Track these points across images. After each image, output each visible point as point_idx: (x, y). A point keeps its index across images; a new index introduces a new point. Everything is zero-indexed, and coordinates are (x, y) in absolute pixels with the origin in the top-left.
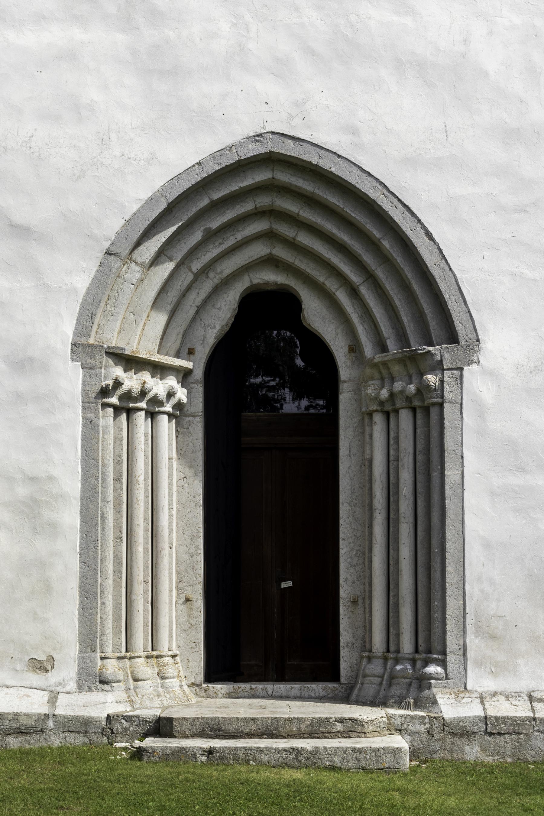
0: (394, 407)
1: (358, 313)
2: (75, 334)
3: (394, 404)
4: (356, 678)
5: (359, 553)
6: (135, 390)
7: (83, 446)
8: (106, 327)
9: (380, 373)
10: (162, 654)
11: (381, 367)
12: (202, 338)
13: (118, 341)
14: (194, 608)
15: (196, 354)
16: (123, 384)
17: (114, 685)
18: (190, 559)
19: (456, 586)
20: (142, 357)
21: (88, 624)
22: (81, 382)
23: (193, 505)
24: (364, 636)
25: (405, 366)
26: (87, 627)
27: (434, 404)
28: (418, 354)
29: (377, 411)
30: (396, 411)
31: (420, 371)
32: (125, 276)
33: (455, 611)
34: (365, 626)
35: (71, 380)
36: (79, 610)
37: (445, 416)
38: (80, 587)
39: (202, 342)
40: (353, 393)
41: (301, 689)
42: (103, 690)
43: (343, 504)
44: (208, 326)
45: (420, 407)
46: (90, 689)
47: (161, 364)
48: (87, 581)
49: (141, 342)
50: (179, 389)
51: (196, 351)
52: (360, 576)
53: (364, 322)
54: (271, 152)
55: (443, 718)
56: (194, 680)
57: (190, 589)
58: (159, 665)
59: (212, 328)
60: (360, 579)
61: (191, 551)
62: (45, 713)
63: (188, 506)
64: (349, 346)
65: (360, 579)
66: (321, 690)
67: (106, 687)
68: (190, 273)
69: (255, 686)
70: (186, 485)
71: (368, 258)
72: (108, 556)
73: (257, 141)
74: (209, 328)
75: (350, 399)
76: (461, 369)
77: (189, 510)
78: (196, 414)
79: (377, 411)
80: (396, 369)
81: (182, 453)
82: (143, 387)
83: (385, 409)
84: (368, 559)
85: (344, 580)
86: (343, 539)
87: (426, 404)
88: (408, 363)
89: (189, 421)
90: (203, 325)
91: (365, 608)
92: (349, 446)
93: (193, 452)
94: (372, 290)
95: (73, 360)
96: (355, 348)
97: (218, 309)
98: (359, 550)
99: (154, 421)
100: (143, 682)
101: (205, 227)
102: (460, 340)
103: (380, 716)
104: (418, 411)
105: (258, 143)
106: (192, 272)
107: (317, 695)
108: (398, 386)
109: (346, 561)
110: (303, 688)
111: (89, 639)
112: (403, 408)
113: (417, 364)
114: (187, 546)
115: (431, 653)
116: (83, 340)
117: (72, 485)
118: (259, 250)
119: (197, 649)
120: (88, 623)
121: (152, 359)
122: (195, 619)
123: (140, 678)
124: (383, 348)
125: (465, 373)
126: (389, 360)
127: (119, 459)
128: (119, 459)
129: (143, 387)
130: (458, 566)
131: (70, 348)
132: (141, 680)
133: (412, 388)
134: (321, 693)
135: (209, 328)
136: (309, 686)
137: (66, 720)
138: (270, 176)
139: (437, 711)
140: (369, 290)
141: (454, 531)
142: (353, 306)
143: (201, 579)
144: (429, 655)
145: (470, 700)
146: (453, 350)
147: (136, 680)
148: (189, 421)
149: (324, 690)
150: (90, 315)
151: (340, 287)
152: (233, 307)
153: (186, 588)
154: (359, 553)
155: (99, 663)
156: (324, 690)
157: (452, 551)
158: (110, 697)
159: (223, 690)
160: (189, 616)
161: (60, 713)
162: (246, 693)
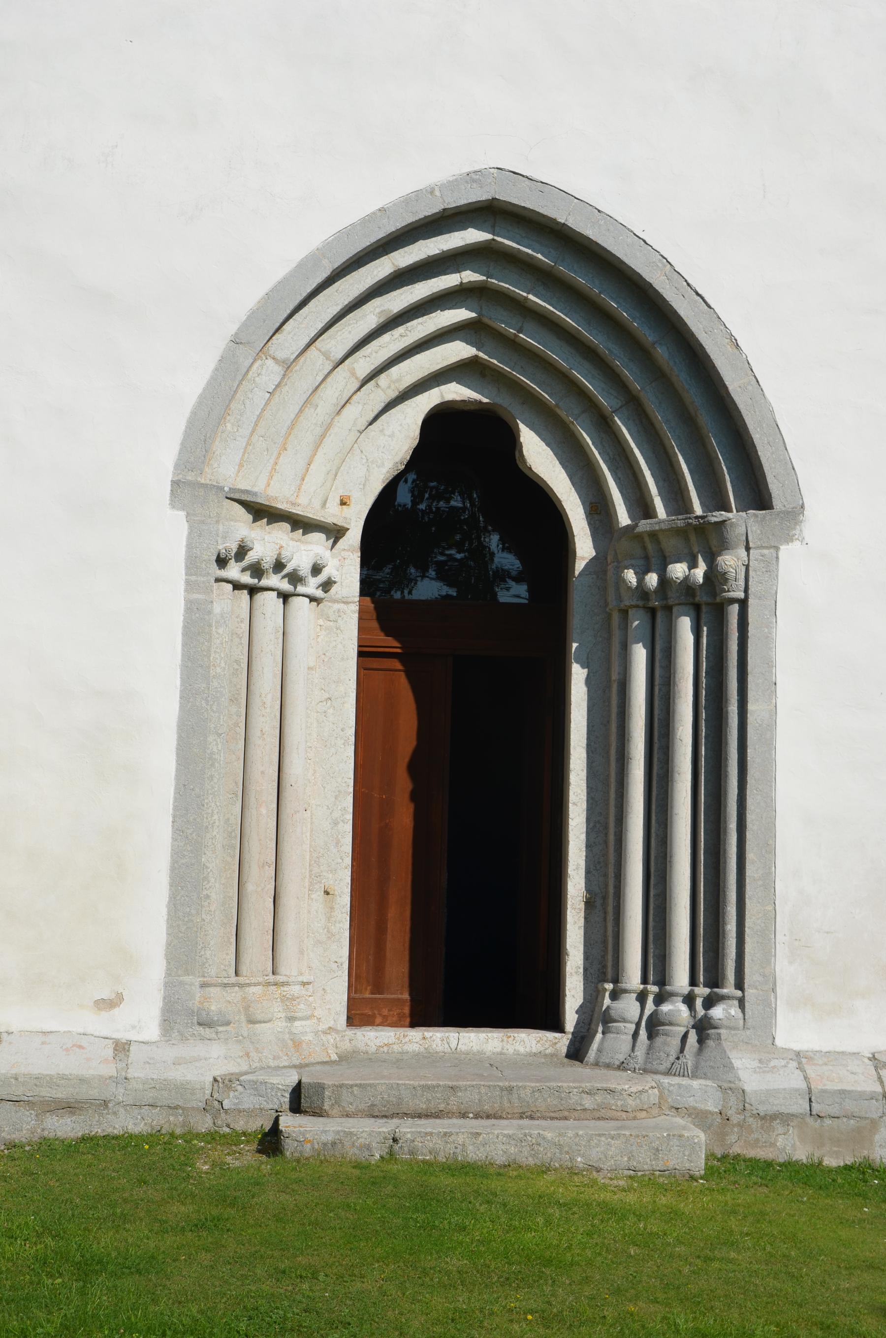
0: (665, 602)
1: (608, 454)
2: (177, 466)
3: (665, 598)
4: (590, 1024)
5: (598, 826)
6: (268, 559)
7: (185, 645)
8: (223, 457)
9: (644, 548)
10: (290, 980)
11: (647, 539)
12: (363, 479)
13: (238, 479)
14: (336, 906)
15: (352, 505)
16: (251, 549)
17: (220, 1029)
18: (332, 829)
19: (760, 883)
20: (280, 507)
21: (183, 930)
22: (184, 543)
23: (340, 742)
24: (603, 957)
25: (687, 539)
26: (181, 935)
27: (733, 601)
28: (710, 523)
29: (637, 606)
30: (668, 609)
31: (710, 548)
32: (257, 379)
33: (759, 921)
34: (605, 942)
35: (166, 539)
36: (168, 906)
37: (750, 620)
38: (173, 869)
39: (361, 486)
40: (594, 576)
41: (503, 1041)
42: (202, 1039)
43: (575, 748)
44: (372, 462)
45: (707, 604)
46: (183, 1038)
47: (306, 520)
48: (184, 861)
49: (272, 482)
50: (330, 559)
51: (353, 500)
52: (599, 863)
53: (617, 468)
54: (494, 199)
55: (743, 1091)
56: (332, 1022)
57: (330, 876)
58: (284, 999)
59: (379, 467)
60: (598, 868)
61: (336, 814)
62: (111, 1074)
63: (333, 743)
64: (591, 503)
65: (598, 868)
66: (534, 1042)
67: (207, 1032)
68: (353, 379)
69: (431, 1034)
70: (331, 711)
71: (629, 373)
72: (217, 821)
73: (474, 181)
74: (374, 466)
75: (589, 586)
76: (777, 549)
77: (333, 750)
78: (350, 600)
79: (637, 606)
80: (670, 544)
81: (326, 660)
82: (279, 554)
83: (651, 604)
84: (615, 835)
85: (574, 867)
86: (574, 804)
87: (718, 600)
88: (693, 538)
89: (339, 611)
90: (365, 461)
91: (605, 913)
92: (588, 658)
93: (343, 659)
94: (634, 420)
95: (173, 505)
96: (599, 510)
97: (389, 436)
98: (599, 822)
99: (287, 607)
100: (263, 1025)
101: (382, 308)
102: (774, 504)
103: (649, 1085)
104: (704, 609)
105: (475, 185)
106: (357, 378)
107: (528, 1050)
108: (678, 570)
109: (578, 837)
110: (505, 1039)
111: (183, 953)
112: (680, 604)
113: (708, 540)
114: (328, 808)
115: (718, 987)
116: (190, 477)
117: (164, 706)
118: (458, 351)
119: (340, 972)
120: (183, 929)
121: (294, 511)
122: (337, 925)
123: (259, 1017)
124: (641, 507)
125: (781, 554)
126: (661, 530)
127: (236, 667)
128: (236, 667)
129: (279, 554)
130: (764, 851)
131: (169, 488)
132: (260, 1022)
133: (699, 573)
134: (534, 1045)
135: (374, 466)
136: (516, 1035)
137: (146, 1086)
138: (489, 236)
139: (732, 1080)
140: (629, 419)
141: (759, 797)
142: (601, 443)
143: (348, 861)
144: (716, 990)
145: (783, 1063)
146: (764, 517)
147: (252, 1021)
148: (339, 611)
149: (538, 1042)
150: (202, 438)
151: (583, 412)
152: (412, 435)
153: (324, 874)
154: (598, 826)
155: (198, 994)
156: (538, 1042)
157: (755, 828)
158: (216, 1050)
159: (378, 1041)
160: (329, 919)
161: (136, 1075)
162: (415, 1045)
